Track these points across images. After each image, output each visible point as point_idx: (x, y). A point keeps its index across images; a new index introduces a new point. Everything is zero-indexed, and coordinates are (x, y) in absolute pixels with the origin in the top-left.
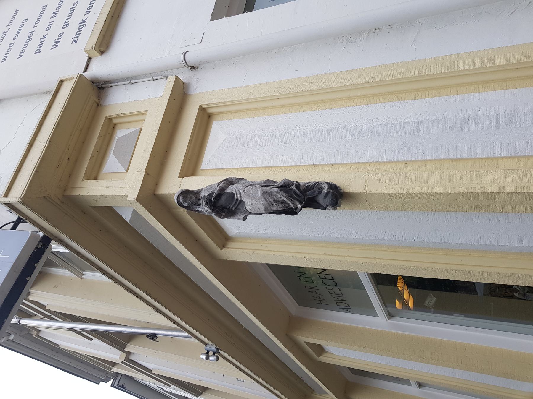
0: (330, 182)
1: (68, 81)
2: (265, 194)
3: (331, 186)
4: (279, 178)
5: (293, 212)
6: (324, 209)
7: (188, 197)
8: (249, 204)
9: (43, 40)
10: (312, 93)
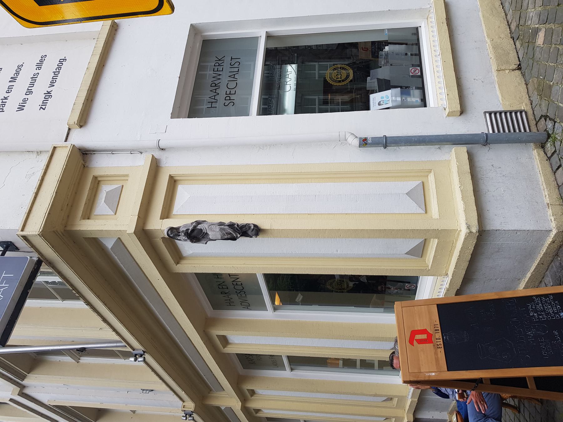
0: (256, 224)
1: (60, 148)
2: (221, 230)
3: (255, 226)
4: (227, 221)
5: (234, 239)
6: (251, 237)
7: (174, 232)
8: (211, 235)
9: (4, 101)
10: (241, 175)
